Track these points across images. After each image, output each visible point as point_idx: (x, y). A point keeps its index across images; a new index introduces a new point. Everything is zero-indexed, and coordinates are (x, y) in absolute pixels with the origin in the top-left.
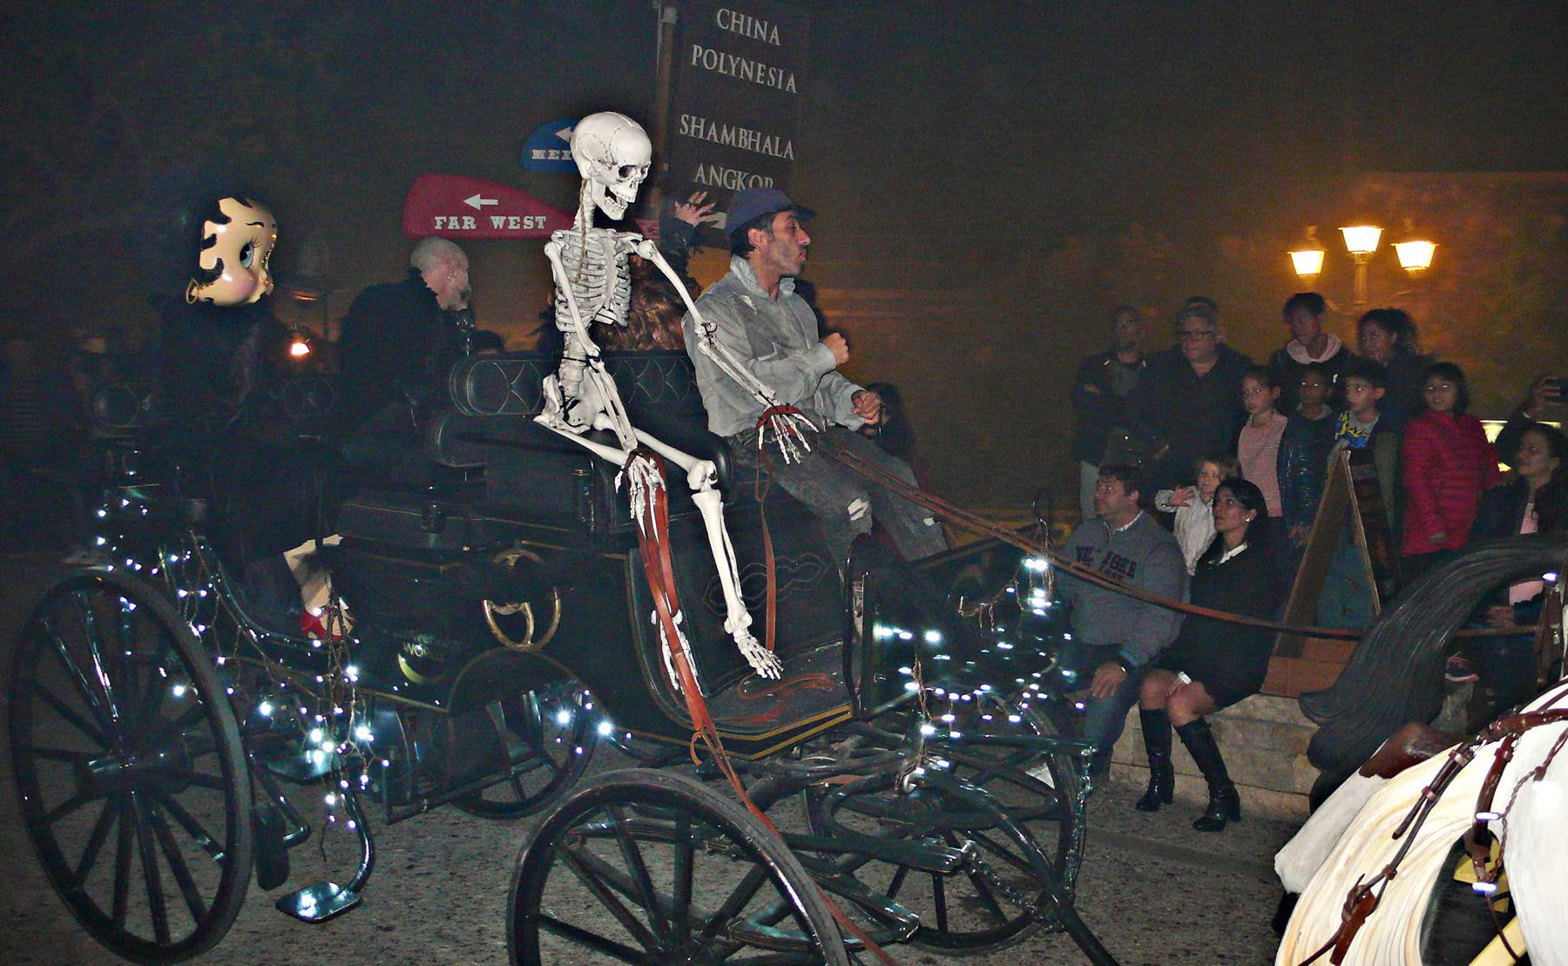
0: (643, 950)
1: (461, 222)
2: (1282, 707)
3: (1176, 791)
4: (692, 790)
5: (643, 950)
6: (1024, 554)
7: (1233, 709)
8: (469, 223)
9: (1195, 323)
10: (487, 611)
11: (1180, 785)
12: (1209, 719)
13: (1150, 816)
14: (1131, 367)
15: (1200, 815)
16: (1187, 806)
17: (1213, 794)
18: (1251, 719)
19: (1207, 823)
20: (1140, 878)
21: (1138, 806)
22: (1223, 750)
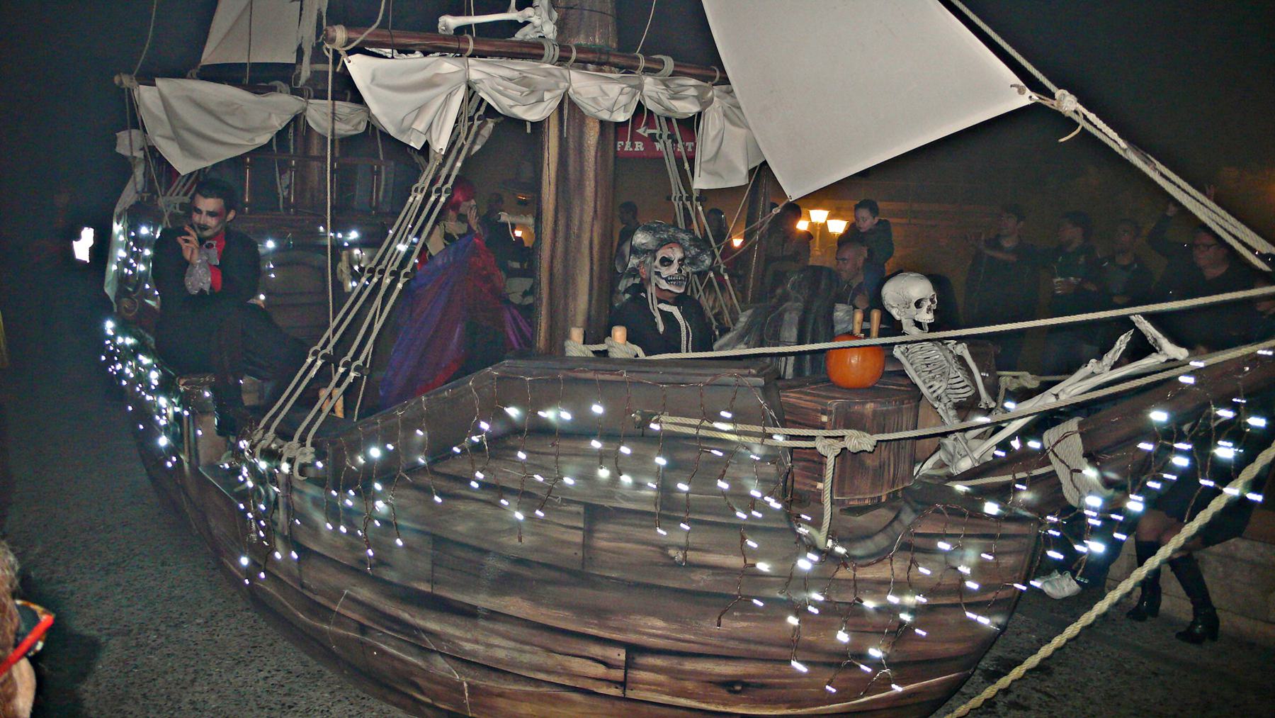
0: (1061, 557)
1: (633, 146)
2: (1261, 550)
3: (1161, 608)
4: (457, 626)
5: (1061, 557)
6: (1195, 385)
7: (1217, 548)
8: (639, 146)
9: (1011, 222)
10: (1265, 352)
11: (1165, 604)
12: (1196, 555)
13: (1138, 625)
14: (1125, 268)
15: (1183, 630)
16: (1170, 621)
17: (1196, 613)
18: (1233, 558)
19: (1188, 636)
20: (1128, 673)
21: (1128, 615)
22: (1206, 578)
